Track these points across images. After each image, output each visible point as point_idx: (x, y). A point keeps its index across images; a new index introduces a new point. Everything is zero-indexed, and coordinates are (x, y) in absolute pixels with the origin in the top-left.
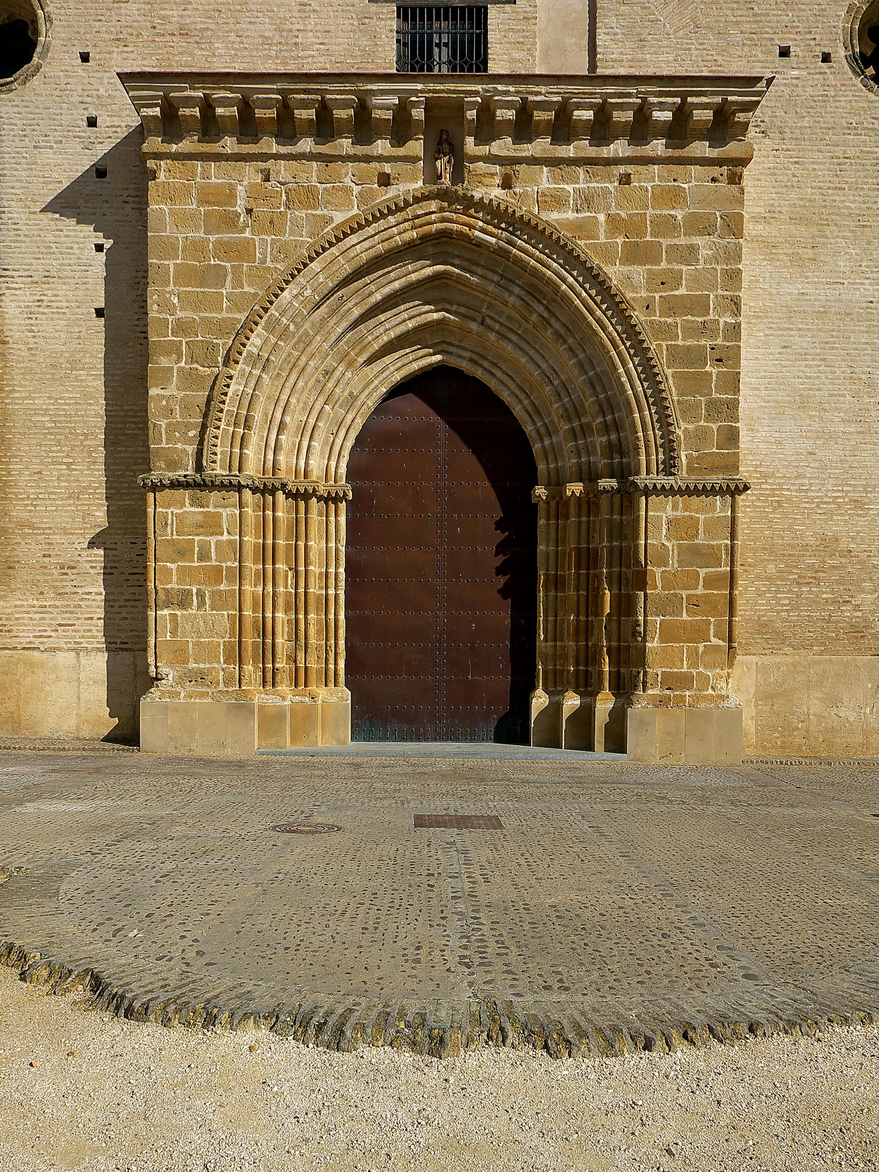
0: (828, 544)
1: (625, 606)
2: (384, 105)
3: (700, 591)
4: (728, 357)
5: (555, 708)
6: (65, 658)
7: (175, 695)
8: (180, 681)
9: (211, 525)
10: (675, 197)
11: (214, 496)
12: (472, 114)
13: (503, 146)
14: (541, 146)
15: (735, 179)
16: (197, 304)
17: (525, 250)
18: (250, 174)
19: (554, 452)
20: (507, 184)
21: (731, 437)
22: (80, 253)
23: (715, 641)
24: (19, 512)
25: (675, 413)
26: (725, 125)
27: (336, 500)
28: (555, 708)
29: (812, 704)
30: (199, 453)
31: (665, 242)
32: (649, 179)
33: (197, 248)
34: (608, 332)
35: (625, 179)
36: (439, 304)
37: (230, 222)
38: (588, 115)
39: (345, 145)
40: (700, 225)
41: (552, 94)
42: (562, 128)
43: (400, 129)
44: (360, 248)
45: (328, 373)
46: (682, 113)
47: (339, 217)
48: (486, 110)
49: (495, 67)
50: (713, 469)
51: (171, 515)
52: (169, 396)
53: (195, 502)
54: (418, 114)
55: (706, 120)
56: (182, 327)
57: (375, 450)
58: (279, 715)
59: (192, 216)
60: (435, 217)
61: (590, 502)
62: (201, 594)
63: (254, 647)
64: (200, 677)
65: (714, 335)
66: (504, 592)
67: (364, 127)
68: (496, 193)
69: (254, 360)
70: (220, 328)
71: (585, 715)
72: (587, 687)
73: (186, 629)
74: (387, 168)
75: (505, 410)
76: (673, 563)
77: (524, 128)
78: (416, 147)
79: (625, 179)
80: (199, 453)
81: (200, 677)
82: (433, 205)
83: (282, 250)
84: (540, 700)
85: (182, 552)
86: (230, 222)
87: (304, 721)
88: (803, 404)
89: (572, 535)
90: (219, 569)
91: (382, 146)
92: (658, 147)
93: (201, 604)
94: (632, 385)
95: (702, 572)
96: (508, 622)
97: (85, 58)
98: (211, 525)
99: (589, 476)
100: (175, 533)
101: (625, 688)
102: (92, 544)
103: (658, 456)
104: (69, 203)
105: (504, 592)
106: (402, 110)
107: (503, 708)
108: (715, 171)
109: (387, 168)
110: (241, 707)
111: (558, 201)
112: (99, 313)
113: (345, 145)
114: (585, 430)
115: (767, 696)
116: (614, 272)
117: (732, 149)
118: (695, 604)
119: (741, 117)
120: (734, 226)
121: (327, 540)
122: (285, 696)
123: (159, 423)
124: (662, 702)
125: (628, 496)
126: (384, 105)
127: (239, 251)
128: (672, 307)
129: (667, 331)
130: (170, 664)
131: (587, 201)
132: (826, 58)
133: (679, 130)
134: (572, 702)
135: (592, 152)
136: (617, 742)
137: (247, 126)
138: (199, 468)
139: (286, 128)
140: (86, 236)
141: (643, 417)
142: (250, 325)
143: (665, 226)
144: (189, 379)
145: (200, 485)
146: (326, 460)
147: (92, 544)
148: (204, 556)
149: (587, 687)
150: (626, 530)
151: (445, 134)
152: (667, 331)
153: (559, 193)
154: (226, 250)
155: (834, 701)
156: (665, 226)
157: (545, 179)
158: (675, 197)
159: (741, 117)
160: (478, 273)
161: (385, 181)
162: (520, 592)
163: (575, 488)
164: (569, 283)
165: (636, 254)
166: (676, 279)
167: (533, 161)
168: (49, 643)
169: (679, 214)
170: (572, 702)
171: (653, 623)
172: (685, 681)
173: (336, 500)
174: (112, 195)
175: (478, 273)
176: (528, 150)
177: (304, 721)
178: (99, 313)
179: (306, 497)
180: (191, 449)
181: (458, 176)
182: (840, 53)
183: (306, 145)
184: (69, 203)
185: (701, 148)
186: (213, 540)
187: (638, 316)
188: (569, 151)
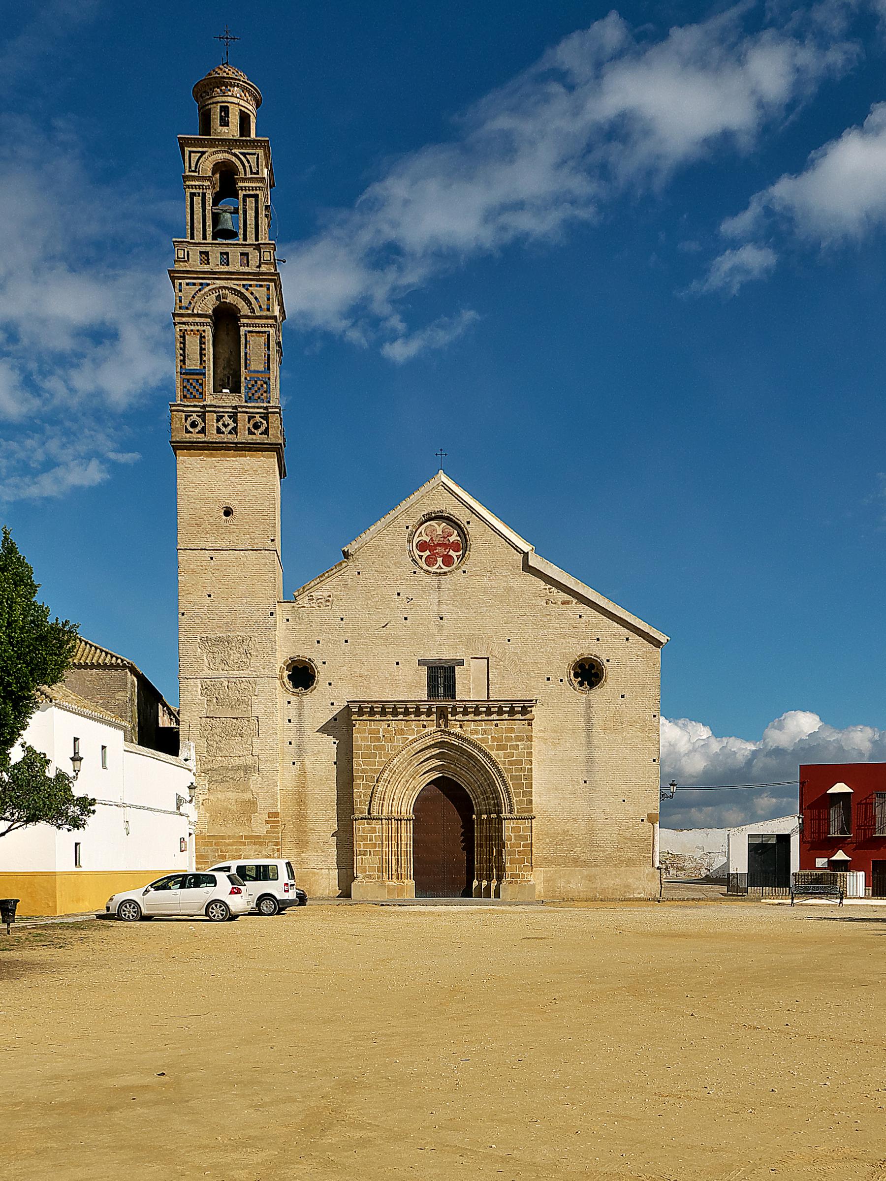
0: (565, 832)
1: (500, 853)
4: (529, 778)
5: (480, 885)
9: (373, 830)
10: (512, 730)
12: (450, 710)
13: (459, 717)
14: (471, 717)
15: (530, 724)
16: (365, 763)
17: (466, 746)
18: (384, 725)
19: (479, 804)
20: (461, 727)
21: (531, 802)
22: (329, 745)
24: (310, 826)
25: (513, 795)
26: (524, 711)
27: (410, 820)
28: (480, 885)
29: (561, 883)
30: (369, 809)
32: (503, 725)
33: (368, 747)
34: (492, 771)
35: (497, 725)
36: (441, 759)
37: (378, 739)
38: (484, 709)
39: (412, 717)
40: (519, 738)
41: (474, 705)
42: (477, 712)
43: (429, 713)
44: (418, 746)
45: (407, 782)
46: (512, 708)
47: (411, 738)
49: (457, 699)
50: (525, 812)
51: (361, 828)
52: (360, 792)
54: (434, 710)
55: (520, 710)
56: (363, 771)
57: (422, 803)
58: (394, 888)
59: (367, 737)
60: (439, 737)
61: (489, 820)
63: (385, 868)
64: (370, 877)
66: (463, 849)
67: (418, 712)
68: (458, 730)
69: (385, 780)
70: (375, 771)
71: (488, 887)
72: (489, 878)
73: (365, 863)
74: (425, 723)
76: (513, 841)
77: (465, 712)
78: (434, 717)
79: (497, 725)
80: (369, 809)
81: (370, 877)
82: (439, 733)
84: (475, 883)
85: (365, 839)
86: (378, 739)
87: (401, 890)
88: (556, 789)
91: (423, 717)
92: (506, 716)
94: (500, 787)
97: (330, 684)
98: (373, 830)
99: (489, 813)
101: (500, 879)
102: (333, 836)
103: (508, 808)
104: (324, 730)
105: (463, 849)
106: (430, 709)
107: (465, 886)
108: (524, 722)
109: (425, 723)
110: (383, 886)
112: (335, 763)
113: (412, 717)
115: (546, 881)
116: (493, 754)
117: (528, 716)
119: (529, 709)
120: (530, 739)
121: (406, 833)
122: (394, 883)
123: (356, 799)
124: (511, 882)
125: (500, 820)
128: (511, 763)
129: (510, 771)
130: (361, 873)
131: (485, 732)
132: (561, 681)
133: (512, 712)
134: (485, 883)
135: (486, 718)
136: (497, 895)
137: (383, 712)
138: (369, 813)
139: (395, 713)
140: (331, 739)
141: (503, 796)
142: (383, 771)
143: (509, 739)
144: (366, 787)
145: (370, 818)
146: (406, 807)
147: (333, 836)
149: (489, 878)
150: (500, 830)
151: (442, 714)
152: (510, 771)
153: (476, 732)
155: (569, 882)
156: (509, 739)
157: (472, 726)
158: (512, 730)
159: (529, 709)
160: (451, 752)
161: (424, 726)
162: (469, 848)
163: (484, 816)
164: (480, 756)
165: (500, 748)
167: (468, 721)
170: (485, 883)
171: (506, 858)
172: (518, 876)
173: (410, 820)
174: (341, 726)
175: (451, 752)
176: (467, 718)
177: (401, 890)
178: (335, 763)
179: (401, 820)
180: (367, 808)
181: (446, 726)
183: (401, 717)
184: (324, 730)
185: (518, 716)
187: (501, 766)
188: (479, 718)
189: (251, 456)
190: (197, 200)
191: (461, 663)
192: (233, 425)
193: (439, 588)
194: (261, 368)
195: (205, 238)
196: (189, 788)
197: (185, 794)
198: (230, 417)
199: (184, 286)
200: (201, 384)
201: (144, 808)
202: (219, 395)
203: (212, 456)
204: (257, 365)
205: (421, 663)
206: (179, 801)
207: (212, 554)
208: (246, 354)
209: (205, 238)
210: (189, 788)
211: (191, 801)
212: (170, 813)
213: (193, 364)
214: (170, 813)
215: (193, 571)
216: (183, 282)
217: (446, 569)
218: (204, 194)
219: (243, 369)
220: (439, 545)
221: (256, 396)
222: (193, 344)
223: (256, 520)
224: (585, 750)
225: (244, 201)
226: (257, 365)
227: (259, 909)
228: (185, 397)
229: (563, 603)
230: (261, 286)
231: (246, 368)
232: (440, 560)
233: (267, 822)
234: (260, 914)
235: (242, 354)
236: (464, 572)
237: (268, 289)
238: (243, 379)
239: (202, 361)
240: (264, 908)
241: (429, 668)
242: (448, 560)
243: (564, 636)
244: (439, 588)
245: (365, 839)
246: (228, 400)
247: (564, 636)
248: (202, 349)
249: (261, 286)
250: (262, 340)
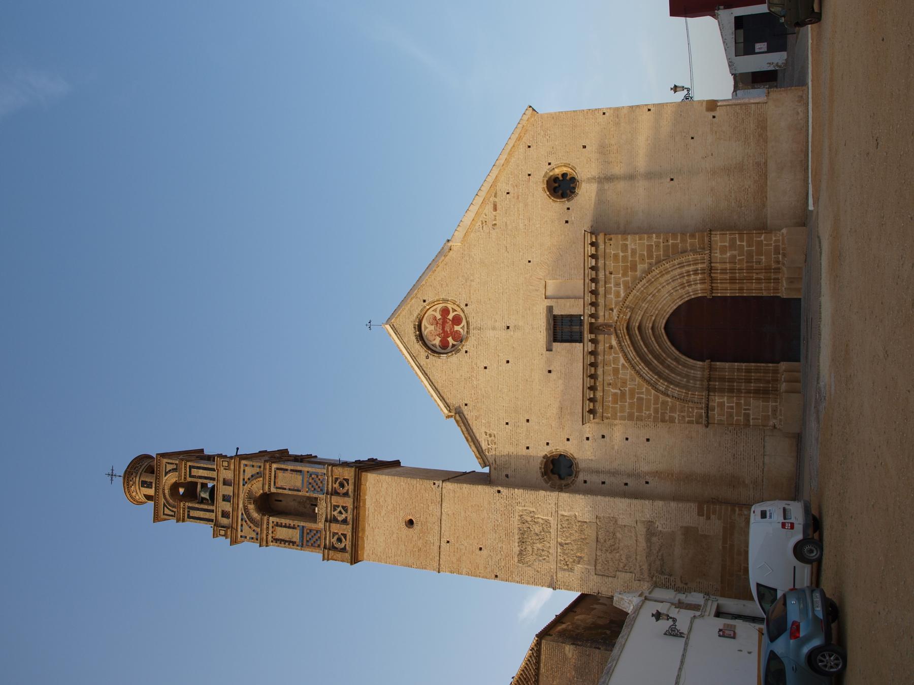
2: (590, 346)
3: (745, 243)
6: (767, 460)
7: (780, 420)
8: (776, 418)
9: (721, 405)
10: (616, 256)
11: (711, 404)
16: (648, 408)
23: (763, 238)
31: (630, 259)
32: (611, 265)
37: (623, 394)
48: (591, 316)
50: (703, 240)
53: (714, 410)
62: (745, 410)
65: (659, 243)
75: (680, 306)
81: (774, 411)
83: (633, 380)
89: (724, 285)
90: (737, 403)
93: (748, 409)
95: (738, 243)
96: (593, 195)
100: (210, 508)
106: (592, 341)
111: (617, 295)
114: (688, 282)
118: (749, 245)
121: (725, 367)
124: (784, 255)
126: (590, 346)
127: (632, 392)
148: (732, 408)
154: (632, 397)
157: (612, 296)
165: (634, 268)
166: (642, 256)
168: (761, 464)
169: (621, 254)
182: (568, 204)
186: (726, 404)
189: (365, 494)
190: (193, 513)
191: (550, 309)
192: (340, 509)
193: (480, 329)
194: (300, 477)
195: (212, 511)
196: (657, 619)
197: (665, 624)
198: (335, 510)
199: (243, 534)
200: (311, 531)
201: (682, 662)
202: (319, 517)
203: (364, 530)
204: (296, 481)
205: (549, 349)
206: (673, 633)
207: (444, 540)
208: (290, 489)
209: (212, 511)
210: (657, 619)
211: (674, 620)
212: (686, 644)
213: (295, 535)
214: (686, 644)
215: (459, 560)
216: (239, 534)
217: (464, 323)
218: (189, 508)
219: (300, 493)
220: (443, 328)
221: (321, 485)
222: (282, 533)
223: (417, 496)
224: (703, 281)
225: (194, 477)
226: (296, 481)
227: (814, 560)
228: (319, 546)
229: (495, 209)
230: (244, 471)
231: (299, 491)
232: (457, 328)
233: (708, 518)
234: (819, 561)
235: (290, 493)
236: (466, 305)
237: (246, 465)
238: (308, 494)
239: (294, 528)
240: (814, 555)
241: (555, 341)
242: (457, 320)
243: (526, 205)
244: (480, 329)
245: (730, 415)
246: (321, 510)
247: (526, 205)
248: (285, 526)
249: (244, 471)
250: (280, 474)
